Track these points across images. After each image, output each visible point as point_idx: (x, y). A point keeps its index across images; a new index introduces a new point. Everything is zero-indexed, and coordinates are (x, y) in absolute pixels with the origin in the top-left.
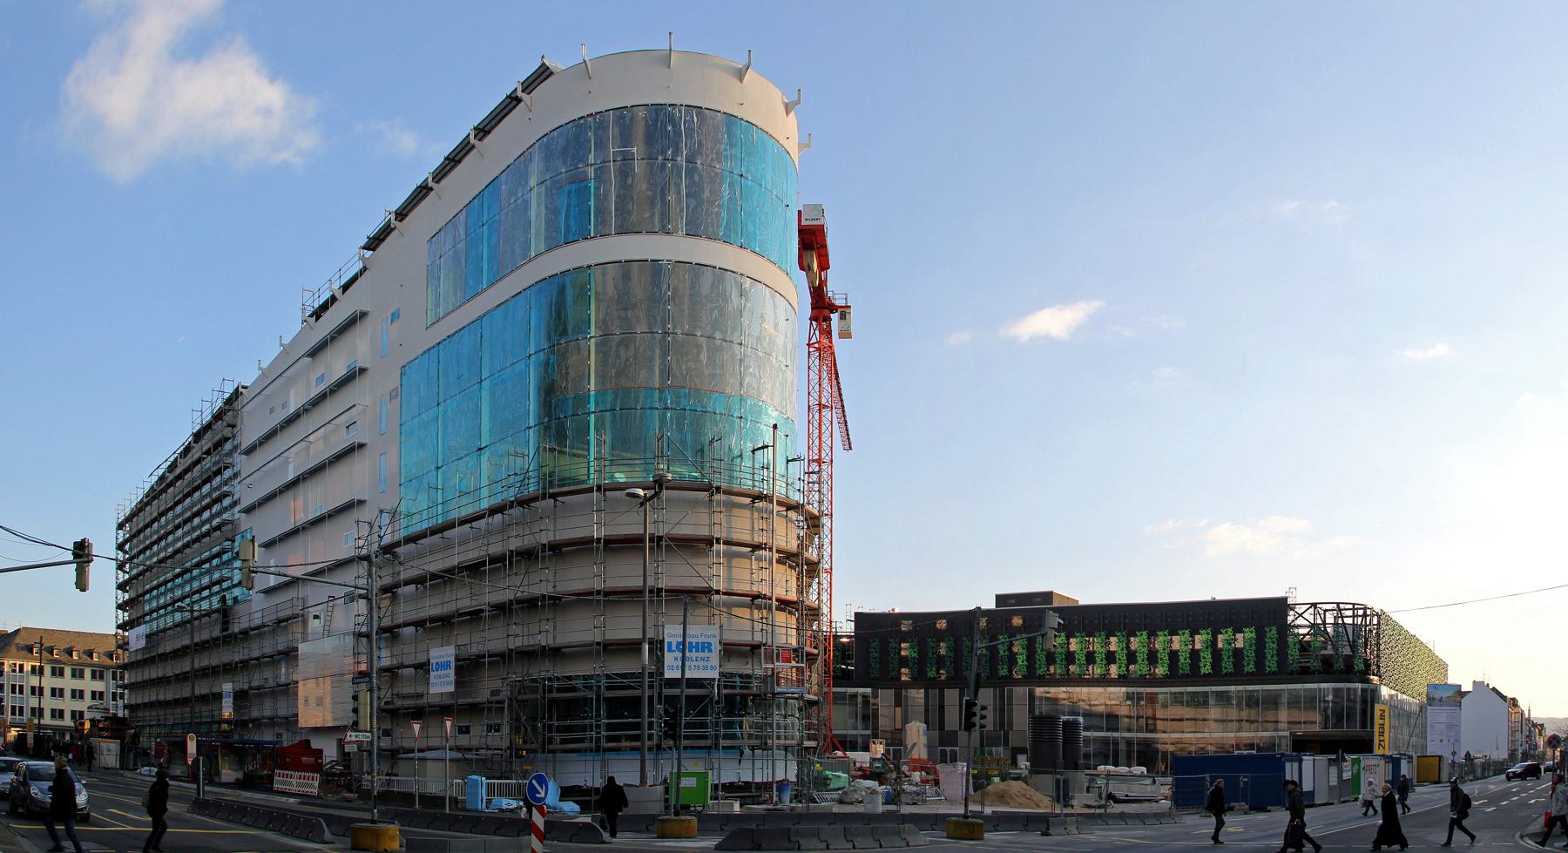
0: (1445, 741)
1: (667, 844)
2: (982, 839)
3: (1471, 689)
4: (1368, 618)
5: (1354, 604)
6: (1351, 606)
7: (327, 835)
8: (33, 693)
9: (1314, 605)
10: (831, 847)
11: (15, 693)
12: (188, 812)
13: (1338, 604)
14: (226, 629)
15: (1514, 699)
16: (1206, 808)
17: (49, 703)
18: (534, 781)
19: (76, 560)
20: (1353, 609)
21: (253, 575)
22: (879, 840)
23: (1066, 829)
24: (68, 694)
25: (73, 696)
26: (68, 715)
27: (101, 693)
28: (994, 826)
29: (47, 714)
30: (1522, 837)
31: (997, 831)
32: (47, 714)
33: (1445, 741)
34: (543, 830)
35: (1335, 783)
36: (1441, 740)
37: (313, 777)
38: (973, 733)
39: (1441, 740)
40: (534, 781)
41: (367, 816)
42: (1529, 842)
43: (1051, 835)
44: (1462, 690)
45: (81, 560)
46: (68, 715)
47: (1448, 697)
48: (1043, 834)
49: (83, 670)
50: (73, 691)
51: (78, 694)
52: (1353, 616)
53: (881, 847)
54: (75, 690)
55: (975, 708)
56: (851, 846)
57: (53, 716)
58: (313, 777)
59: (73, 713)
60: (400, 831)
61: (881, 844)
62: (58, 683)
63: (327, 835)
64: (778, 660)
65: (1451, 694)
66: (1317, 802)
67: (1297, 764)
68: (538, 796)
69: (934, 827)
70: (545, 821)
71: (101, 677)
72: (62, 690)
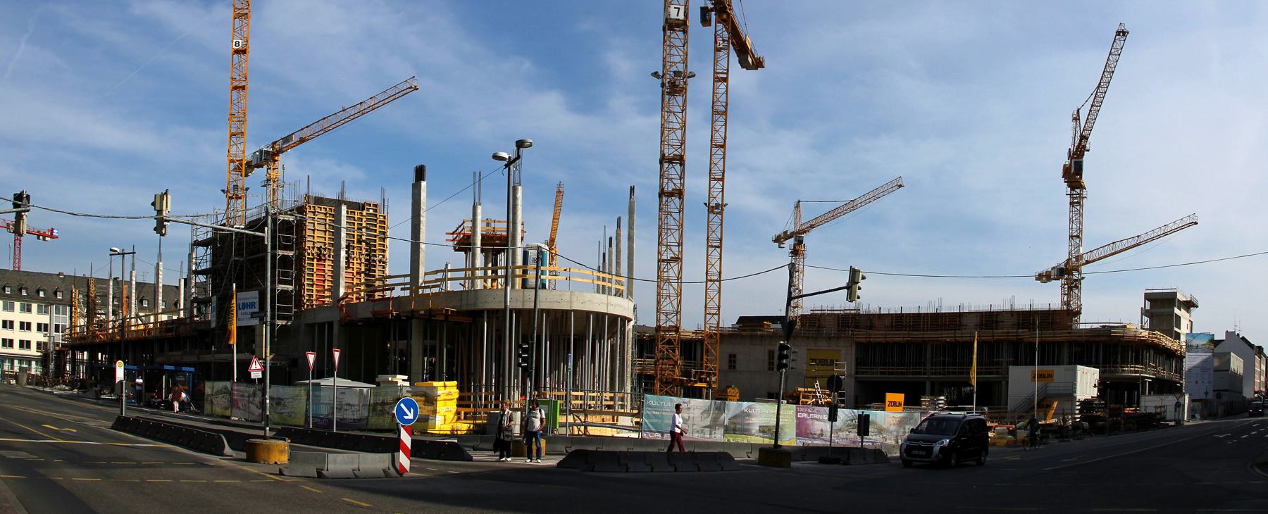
1: (245, 468)
2: (789, 466)
3: (1224, 339)
7: (228, 450)
11: (58, 332)
12: (113, 428)
14: (900, 404)
16: (211, 363)
18: (402, 405)
19: (15, 210)
21: (165, 223)
23: (864, 459)
24: (17, 325)
26: (34, 346)
27: (46, 326)
28: (747, 453)
31: (804, 460)
34: (410, 447)
36: (1197, 382)
39: (1197, 382)
40: (402, 405)
41: (261, 433)
43: (851, 465)
44: (1215, 339)
45: (20, 209)
46: (34, 346)
47: (1202, 345)
49: (31, 305)
50: (22, 324)
51: (25, 326)
53: (699, 470)
54: (23, 323)
56: (673, 469)
59: (39, 344)
60: (290, 446)
62: (26, 317)
63: (228, 450)
64: (1007, 409)
65: (1204, 343)
66: (503, 307)
68: (406, 417)
69: (750, 455)
70: (412, 440)
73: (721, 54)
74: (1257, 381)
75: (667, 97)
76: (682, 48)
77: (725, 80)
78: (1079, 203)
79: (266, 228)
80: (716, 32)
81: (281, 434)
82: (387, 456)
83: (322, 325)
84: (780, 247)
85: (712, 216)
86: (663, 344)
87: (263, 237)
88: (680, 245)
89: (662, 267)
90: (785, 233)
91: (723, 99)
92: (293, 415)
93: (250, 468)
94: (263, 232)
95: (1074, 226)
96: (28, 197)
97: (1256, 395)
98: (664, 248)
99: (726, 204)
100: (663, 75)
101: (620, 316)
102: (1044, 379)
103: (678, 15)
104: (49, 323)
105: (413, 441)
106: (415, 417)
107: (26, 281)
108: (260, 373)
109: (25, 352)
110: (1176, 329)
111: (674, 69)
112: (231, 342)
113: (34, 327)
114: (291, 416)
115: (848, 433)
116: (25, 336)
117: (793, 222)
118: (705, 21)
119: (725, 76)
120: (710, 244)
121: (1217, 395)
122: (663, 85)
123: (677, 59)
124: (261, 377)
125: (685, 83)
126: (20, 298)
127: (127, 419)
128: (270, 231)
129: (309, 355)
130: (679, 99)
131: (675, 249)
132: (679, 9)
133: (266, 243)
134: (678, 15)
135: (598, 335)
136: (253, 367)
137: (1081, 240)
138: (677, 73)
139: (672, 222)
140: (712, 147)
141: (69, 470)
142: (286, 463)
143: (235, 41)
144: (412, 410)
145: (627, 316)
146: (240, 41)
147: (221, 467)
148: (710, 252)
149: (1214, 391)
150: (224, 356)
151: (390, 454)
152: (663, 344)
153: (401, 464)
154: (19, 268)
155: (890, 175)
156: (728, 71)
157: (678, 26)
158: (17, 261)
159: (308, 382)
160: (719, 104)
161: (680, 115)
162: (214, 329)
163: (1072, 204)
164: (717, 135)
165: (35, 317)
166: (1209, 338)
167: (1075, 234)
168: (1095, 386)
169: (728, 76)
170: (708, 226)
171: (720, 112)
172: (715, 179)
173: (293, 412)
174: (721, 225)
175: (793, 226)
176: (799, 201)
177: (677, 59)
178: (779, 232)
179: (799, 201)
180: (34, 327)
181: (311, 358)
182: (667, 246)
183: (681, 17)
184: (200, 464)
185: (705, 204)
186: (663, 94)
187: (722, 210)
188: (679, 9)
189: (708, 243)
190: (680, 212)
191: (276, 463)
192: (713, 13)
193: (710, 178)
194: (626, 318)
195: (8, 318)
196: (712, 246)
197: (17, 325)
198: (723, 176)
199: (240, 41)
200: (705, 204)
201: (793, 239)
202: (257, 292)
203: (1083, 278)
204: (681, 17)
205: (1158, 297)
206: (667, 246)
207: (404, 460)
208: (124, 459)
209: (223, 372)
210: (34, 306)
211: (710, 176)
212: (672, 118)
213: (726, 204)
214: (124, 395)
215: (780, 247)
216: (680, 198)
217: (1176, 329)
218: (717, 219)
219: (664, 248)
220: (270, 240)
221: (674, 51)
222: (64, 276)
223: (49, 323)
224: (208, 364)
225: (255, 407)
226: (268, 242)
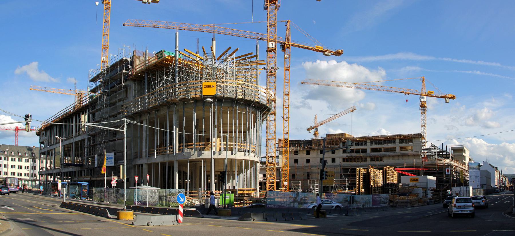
0: (475, 182)
7: (109, 215)
8: (5, 167)
10: (277, 220)
15: (496, 168)
17: (10, 170)
18: (179, 196)
22: (292, 218)
25: (19, 168)
29: (9, 174)
30: (504, 214)
32: (9, 174)
33: (475, 182)
34: (182, 213)
35: (435, 177)
36: (474, 182)
37: (374, 191)
38: (323, 181)
40: (179, 196)
42: (507, 215)
48: (346, 215)
51: (20, 167)
55: (324, 172)
57: (18, 175)
58: (374, 191)
61: (292, 219)
62: (13, 163)
67: (117, 217)
68: (181, 201)
71: (28, 161)
72: (14, 166)
75: (268, 77)
78: (424, 113)
79: (124, 128)
81: (129, 208)
82: (174, 216)
83: (138, 165)
84: (309, 132)
86: (269, 171)
87: (123, 132)
89: (268, 142)
90: (311, 127)
93: (118, 222)
94: (123, 129)
95: (423, 122)
96: (31, 116)
97: (496, 186)
98: (268, 134)
100: (267, 69)
101: (254, 161)
102: (415, 181)
103: (272, 46)
105: (184, 210)
108: (116, 184)
109: (20, 177)
110: (464, 161)
112: (103, 172)
115: (344, 203)
116: (20, 171)
117: (314, 123)
121: (482, 187)
122: (267, 72)
124: (116, 186)
125: (275, 71)
126: (18, 156)
127: (66, 203)
128: (126, 129)
131: (273, 135)
132: (273, 43)
133: (124, 134)
134: (272, 46)
135: (246, 167)
136: (113, 182)
137: (426, 127)
138: (272, 68)
139: (272, 124)
141: (49, 225)
142: (133, 220)
143: (103, 57)
144: (183, 198)
145: (257, 161)
146: (105, 58)
147: (108, 222)
148: (284, 122)
149: (481, 185)
150: (102, 178)
151: (175, 215)
152: (269, 171)
153: (179, 219)
154: (17, 144)
157: (273, 50)
158: (16, 142)
159: (135, 187)
162: (96, 167)
163: (422, 113)
165: (24, 164)
167: (423, 125)
168: (435, 184)
175: (314, 124)
176: (316, 115)
178: (309, 127)
179: (316, 115)
180: (23, 167)
181: (137, 178)
183: (274, 46)
184: (100, 221)
185: (282, 117)
186: (267, 76)
188: (273, 43)
190: (274, 120)
191: (129, 220)
194: (257, 162)
195: (20, 165)
199: (105, 58)
200: (282, 117)
201: (314, 129)
202: (113, 153)
203: (427, 142)
204: (274, 46)
205: (460, 149)
207: (180, 217)
208: (69, 220)
209: (101, 184)
210: (24, 159)
214: (64, 194)
215: (309, 132)
217: (464, 161)
218: (287, 123)
220: (126, 132)
222: (35, 147)
224: (94, 181)
226: (125, 133)
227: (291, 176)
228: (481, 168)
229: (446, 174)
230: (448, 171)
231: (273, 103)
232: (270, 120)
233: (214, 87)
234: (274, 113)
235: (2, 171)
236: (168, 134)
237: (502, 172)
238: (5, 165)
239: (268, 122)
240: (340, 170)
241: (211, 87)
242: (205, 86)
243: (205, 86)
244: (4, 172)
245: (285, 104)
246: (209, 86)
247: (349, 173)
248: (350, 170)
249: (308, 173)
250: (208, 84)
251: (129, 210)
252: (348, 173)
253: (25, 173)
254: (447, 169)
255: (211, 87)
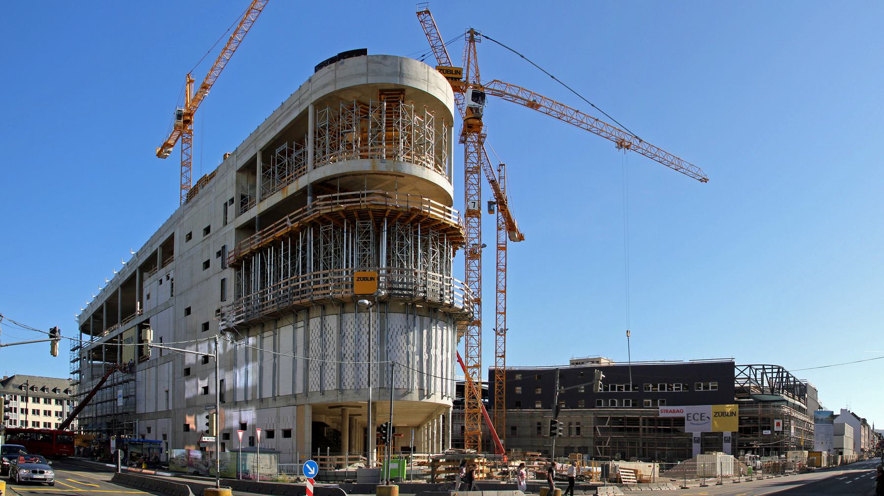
4: (781, 374)
5: (772, 366)
6: (771, 367)
9: (750, 366)
13: (763, 365)
18: (307, 465)
20: (772, 369)
36: (822, 443)
40: (307, 465)
44: (834, 414)
51: (47, 413)
52: (772, 373)
62: (36, 406)
65: (827, 417)
68: (309, 473)
73: (502, 232)
74: (863, 441)
76: (477, 229)
77: (505, 249)
80: (498, 218)
85: (498, 337)
88: (479, 356)
91: (503, 261)
92: (227, 471)
96: (59, 330)
98: (469, 359)
99: (507, 329)
104: (20, 403)
106: (315, 473)
107: (48, 384)
111: (473, 242)
113: (53, 414)
114: (226, 472)
118: (491, 211)
119: (504, 246)
120: (497, 355)
123: (473, 192)
125: (481, 252)
129: (239, 432)
130: (476, 262)
131: (476, 360)
132: (475, 203)
139: (474, 342)
140: (497, 292)
144: (314, 468)
148: (497, 360)
155: (706, 172)
156: (506, 243)
157: (474, 213)
160: (501, 264)
161: (477, 272)
164: (500, 284)
166: (831, 414)
169: (506, 246)
170: (496, 322)
171: (501, 269)
172: (500, 313)
173: (227, 469)
174: (505, 342)
177: (473, 192)
180: (53, 414)
182: (471, 357)
183: (476, 208)
185: (494, 329)
187: (505, 333)
188: (475, 203)
189: (496, 355)
192: (496, 205)
193: (497, 290)
196: (499, 356)
197: (42, 413)
198: (505, 311)
200: (494, 329)
204: (476, 208)
206: (471, 357)
211: (497, 289)
212: (472, 274)
213: (507, 329)
216: (479, 305)
219: (469, 359)
221: (472, 231)
223: (20, 403)
225: (204, 466)
227: (510, 430)
228: (835, 421)
229: (776, 429)
230: (778, 424)
231: (477, 306)
232: (472, 334)
233: (374, 280)
234: (478, 323)
235: (17, 419)
236: (258, 351)
237: (873, 426)
238: (22, 410)
239: (468, 339)
240: (592, 420)
241: (369, 279)
242: (359, 279)
243: (359, 279)
244: (21, 421)
245: (499, 350)
246: (365, 279)
247: (608, 425)
248: (609, 419)
249: (539, 424)
250: (362, 274)
251: (225, 488)
252: (605, 425)
253: (44, 423)
254: (776, 421)
255: (369, 279)
